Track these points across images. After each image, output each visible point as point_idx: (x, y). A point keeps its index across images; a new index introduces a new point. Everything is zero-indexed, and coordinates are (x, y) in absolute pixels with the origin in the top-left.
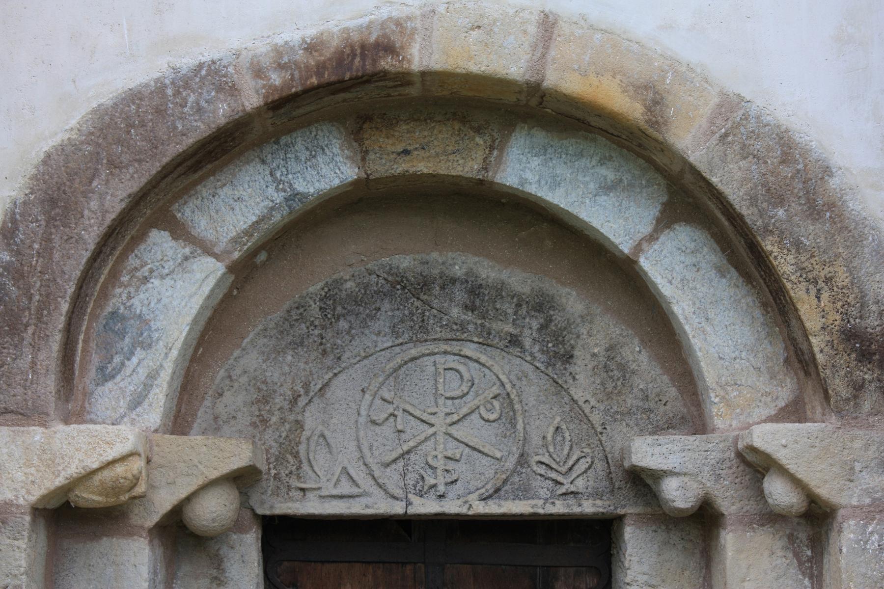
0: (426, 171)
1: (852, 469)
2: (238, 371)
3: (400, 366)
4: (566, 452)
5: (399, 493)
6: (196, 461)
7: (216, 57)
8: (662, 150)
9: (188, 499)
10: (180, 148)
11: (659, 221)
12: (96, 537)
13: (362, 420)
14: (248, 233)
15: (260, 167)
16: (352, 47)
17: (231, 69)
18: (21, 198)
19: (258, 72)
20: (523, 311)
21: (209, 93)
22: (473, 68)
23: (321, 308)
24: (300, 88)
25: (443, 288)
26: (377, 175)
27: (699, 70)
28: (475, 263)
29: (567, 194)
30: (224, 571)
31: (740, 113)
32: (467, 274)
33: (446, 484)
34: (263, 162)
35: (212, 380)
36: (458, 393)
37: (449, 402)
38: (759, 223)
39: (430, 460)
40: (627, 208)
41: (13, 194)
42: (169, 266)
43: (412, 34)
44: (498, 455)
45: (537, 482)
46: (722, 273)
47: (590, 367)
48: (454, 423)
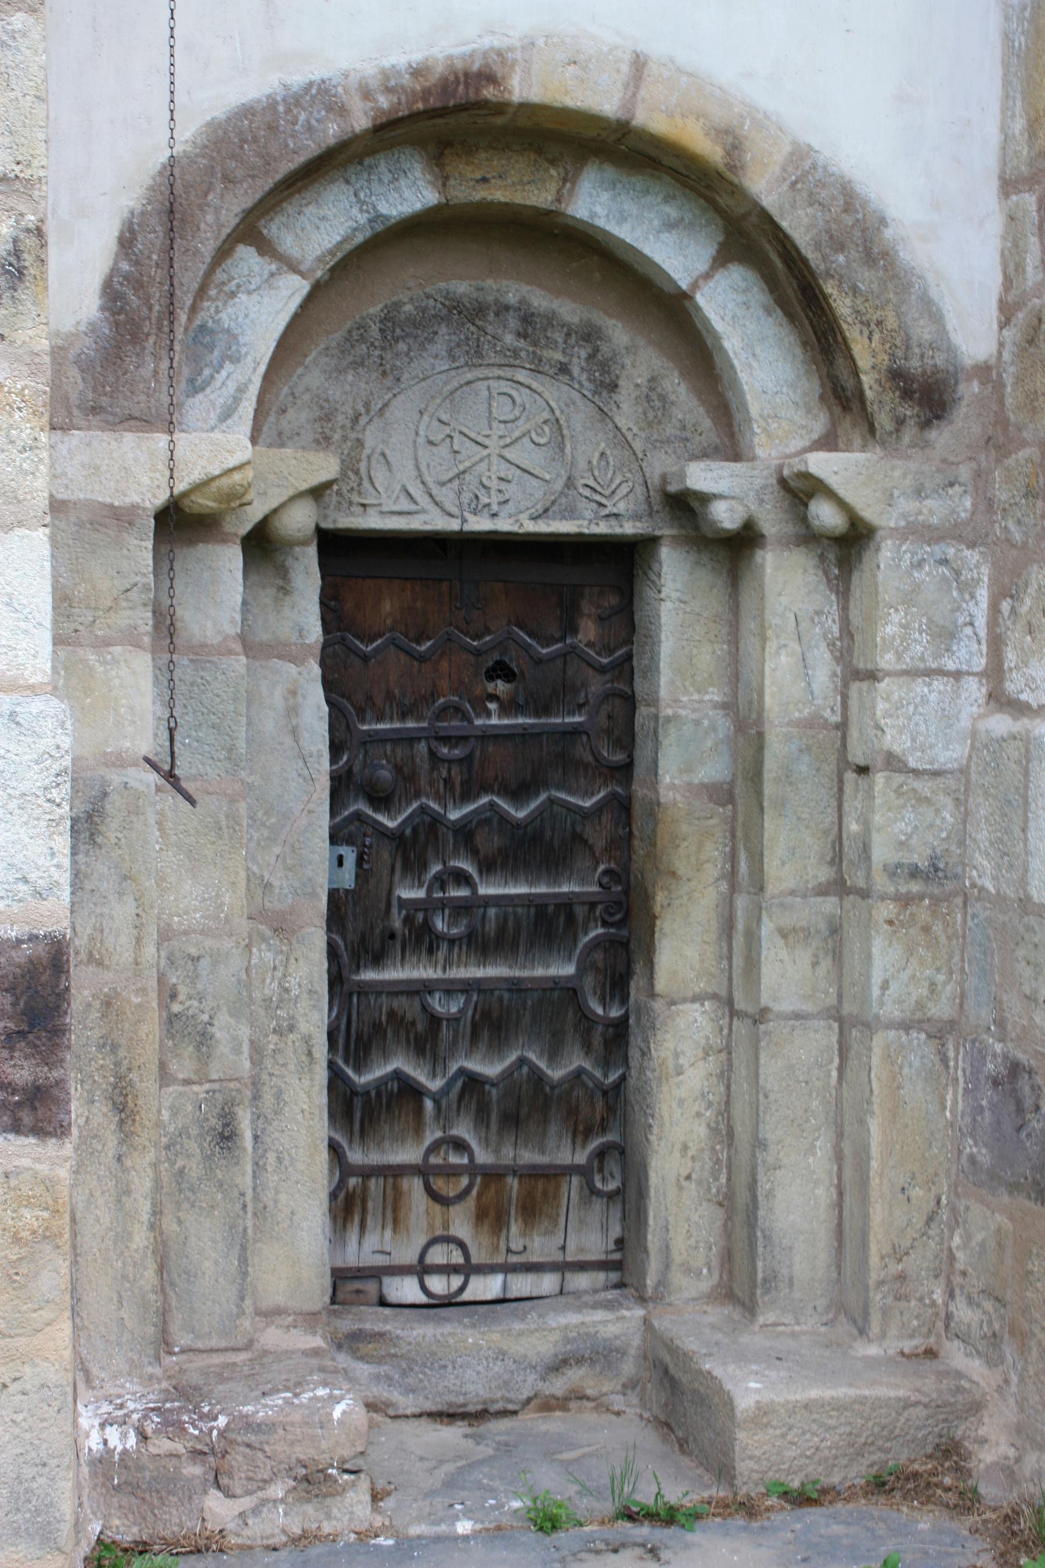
0: (502, 199)
1: (892, 495)
2: (301, 389)
3: (457, 389)
4: (609, 476)
5: (454, 510)
6: (286, 473)
7: (326, 75)
8: (733, 193)
9: (275, 511)
10: (292, 166)
11: (715, 260)
12: (191, 542)
13: (421, 440)
14: (332, 252)
15: (344, 187)
17: (340, 90)
18: (138, 208)
19: (367, 94)
20: (573, 340)
21: (319, 112)
22: (570, 102)
23: (381, 330)
24: (406, 113)
25: (497, 314)
26: (456, 201)
27: (774, 119)
28: (528, 292)
29: (633, 229)
32: (520, 302)
33: (499, 503)
34: (348, 182)
35: (277, 396)
36: (511, 417)
37: (502, 426)
38: (822, 267)
40: (687, 246)
41: (131, 204)
42: (256, 281)
43: (513, 65)
44: (548, 477)
45: (582, 504)
46: (768, 312)
47: (633, 396)
48: (507, 446)
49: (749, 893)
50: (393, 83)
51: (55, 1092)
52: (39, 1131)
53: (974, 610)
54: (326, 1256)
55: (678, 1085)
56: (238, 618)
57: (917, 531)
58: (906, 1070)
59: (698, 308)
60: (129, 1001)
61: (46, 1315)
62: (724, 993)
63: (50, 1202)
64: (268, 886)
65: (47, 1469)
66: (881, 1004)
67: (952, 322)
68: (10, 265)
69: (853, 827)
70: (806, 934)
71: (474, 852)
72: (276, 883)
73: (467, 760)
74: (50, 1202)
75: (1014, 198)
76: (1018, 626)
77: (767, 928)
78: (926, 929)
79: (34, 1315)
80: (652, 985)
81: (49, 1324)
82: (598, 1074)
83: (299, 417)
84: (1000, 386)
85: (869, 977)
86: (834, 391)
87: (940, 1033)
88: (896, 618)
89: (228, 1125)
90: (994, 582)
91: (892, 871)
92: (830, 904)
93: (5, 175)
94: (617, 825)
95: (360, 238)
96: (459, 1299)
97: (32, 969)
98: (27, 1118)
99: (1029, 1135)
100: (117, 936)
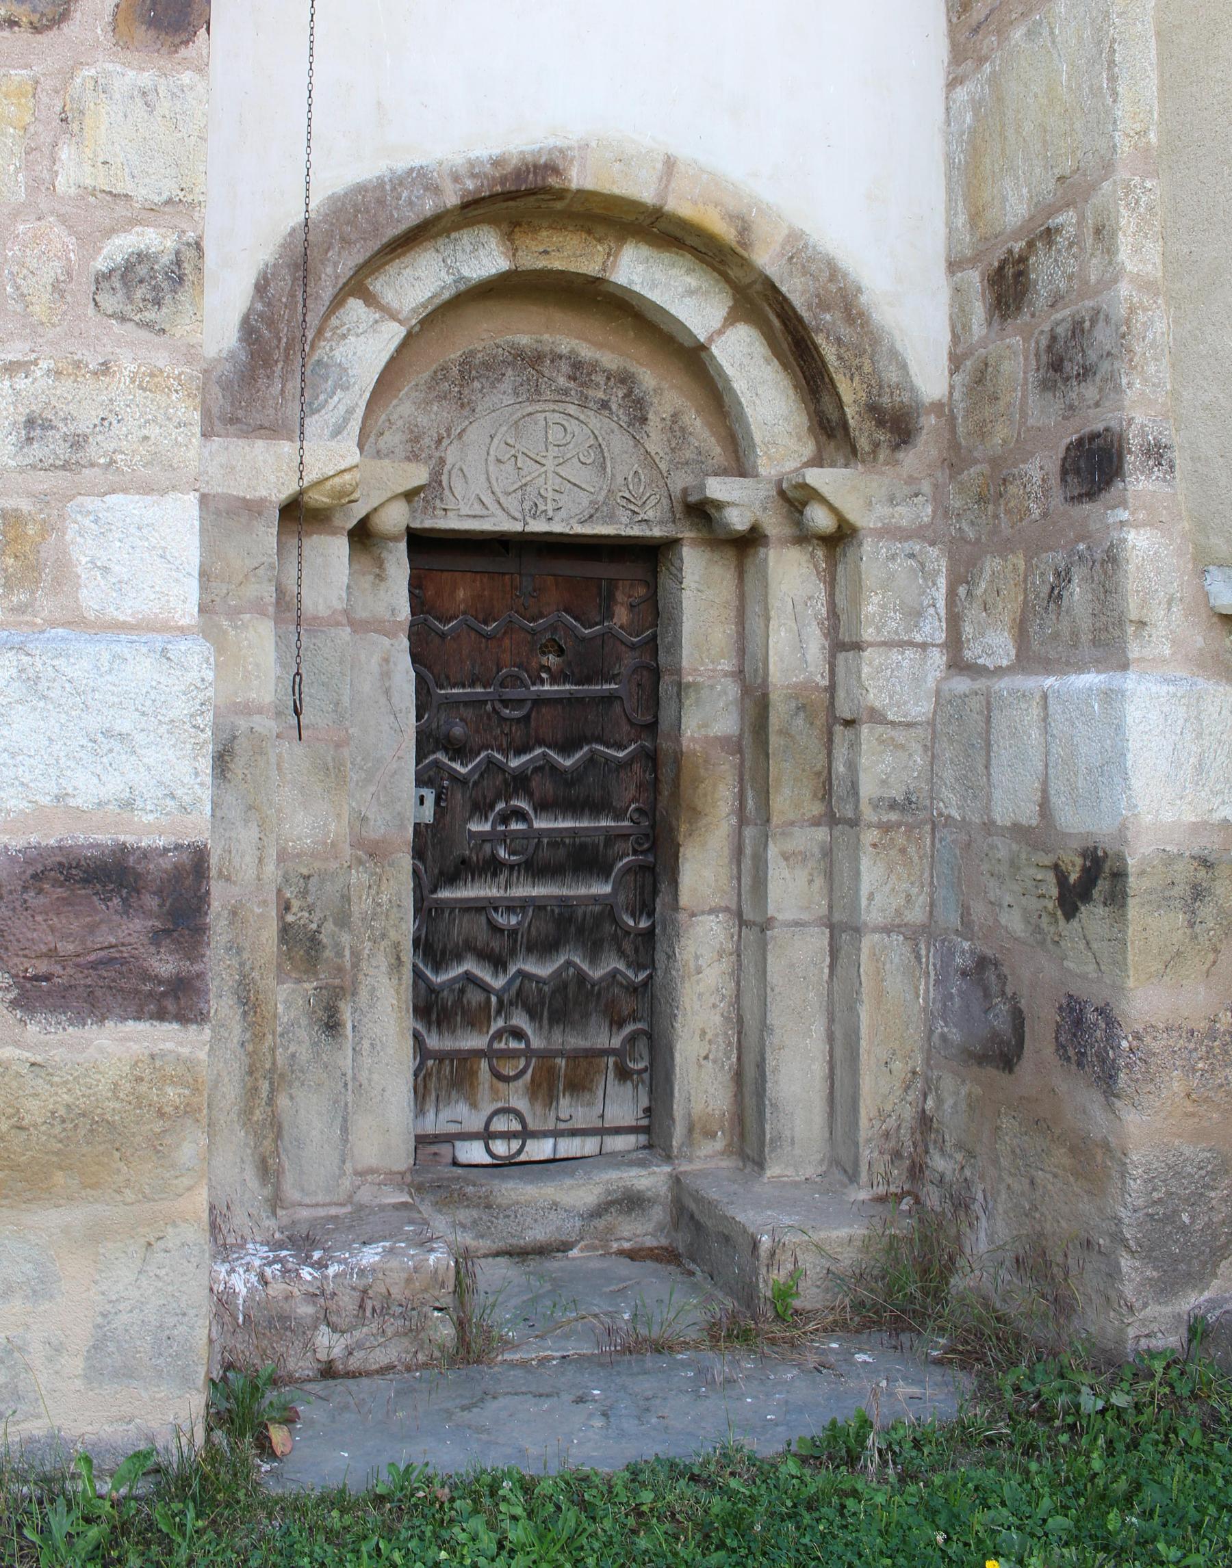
2: (395, 416)
5: (517, 515)
9: (375, 509)
11: (726, 319)
13: (492, 458)
14: (424, 305)
16: (527, 166)
17: (435, 174)
19: (456, 178)
20: (612, 383)
25: (552, 361)
30: (384, 570)
31: (802, 243)
34: (437, 251)
35: (376, 422)
36: (564, 442)
39: (542, 492)
41: (266, 257)
49: (756, 825)
50: (477, 170)
51: (197, 983)
52: (182, 1018)
53: (936, 594)
54: (411, 1125)
55: (698, 982)
56: (344, 595)
57: (890, 532)
58: (888, 966)
59: (713, 357)
60: (252, 911)
61: (186, 1181)
62: (734, 907)
63: (191, 1081)
64: (364, 819)
65: (187, 1319)
66: (869, 912)
67: (913, 368)
68: (172, 272)
69: (840, 768)
70: (804, 857)
71: (530, 795)
72: (371, 816)
73: (527, 718)
74: (191, 1081)
75: (959, 275)
76: (974, 605)
77: (773, 851)
78: (903, 851)
79: (175, 1182)
80: (676, 900)
81: (189, 1189)
82: (630, 974)
83: (393, 439)
84: (952, 419)
85: (857, 891)
86: (821, 423)
87: (913, 935)
88: (875, 599)
89: (333, 1016)
90: (951, 571)
91: (876, 804)
92: (822, 833)
93: (171, 199)
94: (645, 772)
95: (446, 295)
96: (517, 1160)
97: (178, 874)
98: (171, 1005)
99: (996, 1016)
100: (242, 857)
